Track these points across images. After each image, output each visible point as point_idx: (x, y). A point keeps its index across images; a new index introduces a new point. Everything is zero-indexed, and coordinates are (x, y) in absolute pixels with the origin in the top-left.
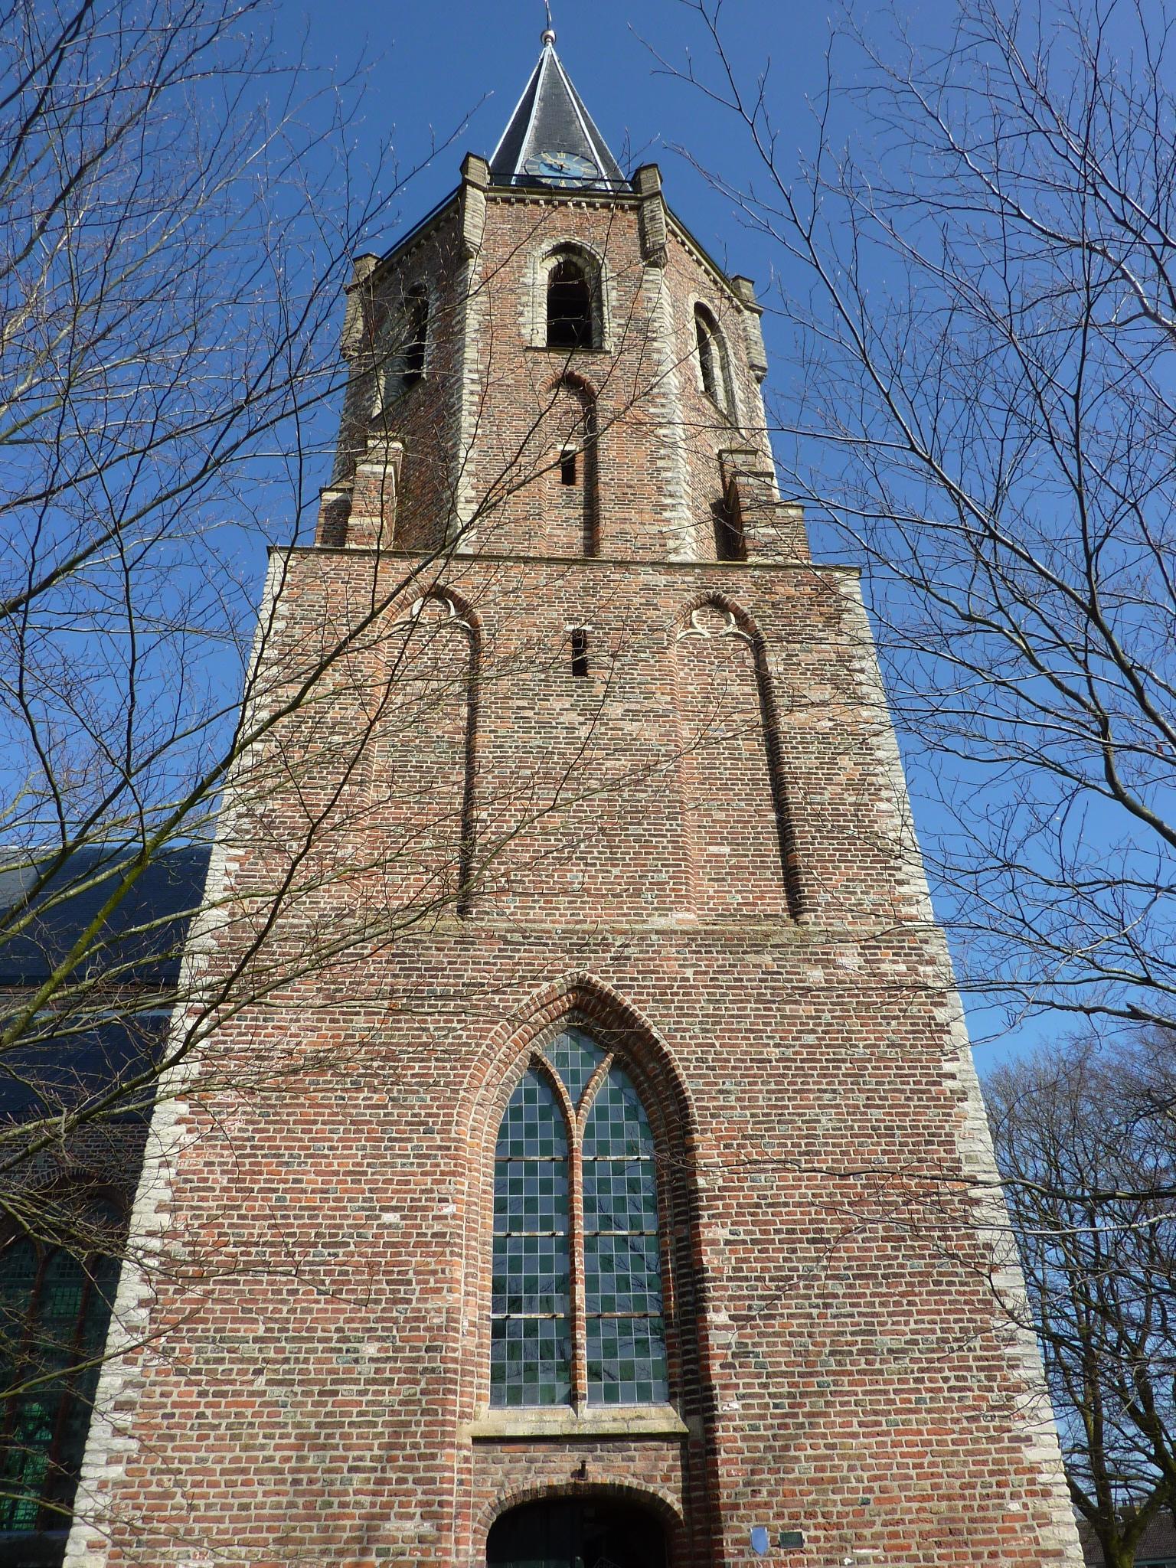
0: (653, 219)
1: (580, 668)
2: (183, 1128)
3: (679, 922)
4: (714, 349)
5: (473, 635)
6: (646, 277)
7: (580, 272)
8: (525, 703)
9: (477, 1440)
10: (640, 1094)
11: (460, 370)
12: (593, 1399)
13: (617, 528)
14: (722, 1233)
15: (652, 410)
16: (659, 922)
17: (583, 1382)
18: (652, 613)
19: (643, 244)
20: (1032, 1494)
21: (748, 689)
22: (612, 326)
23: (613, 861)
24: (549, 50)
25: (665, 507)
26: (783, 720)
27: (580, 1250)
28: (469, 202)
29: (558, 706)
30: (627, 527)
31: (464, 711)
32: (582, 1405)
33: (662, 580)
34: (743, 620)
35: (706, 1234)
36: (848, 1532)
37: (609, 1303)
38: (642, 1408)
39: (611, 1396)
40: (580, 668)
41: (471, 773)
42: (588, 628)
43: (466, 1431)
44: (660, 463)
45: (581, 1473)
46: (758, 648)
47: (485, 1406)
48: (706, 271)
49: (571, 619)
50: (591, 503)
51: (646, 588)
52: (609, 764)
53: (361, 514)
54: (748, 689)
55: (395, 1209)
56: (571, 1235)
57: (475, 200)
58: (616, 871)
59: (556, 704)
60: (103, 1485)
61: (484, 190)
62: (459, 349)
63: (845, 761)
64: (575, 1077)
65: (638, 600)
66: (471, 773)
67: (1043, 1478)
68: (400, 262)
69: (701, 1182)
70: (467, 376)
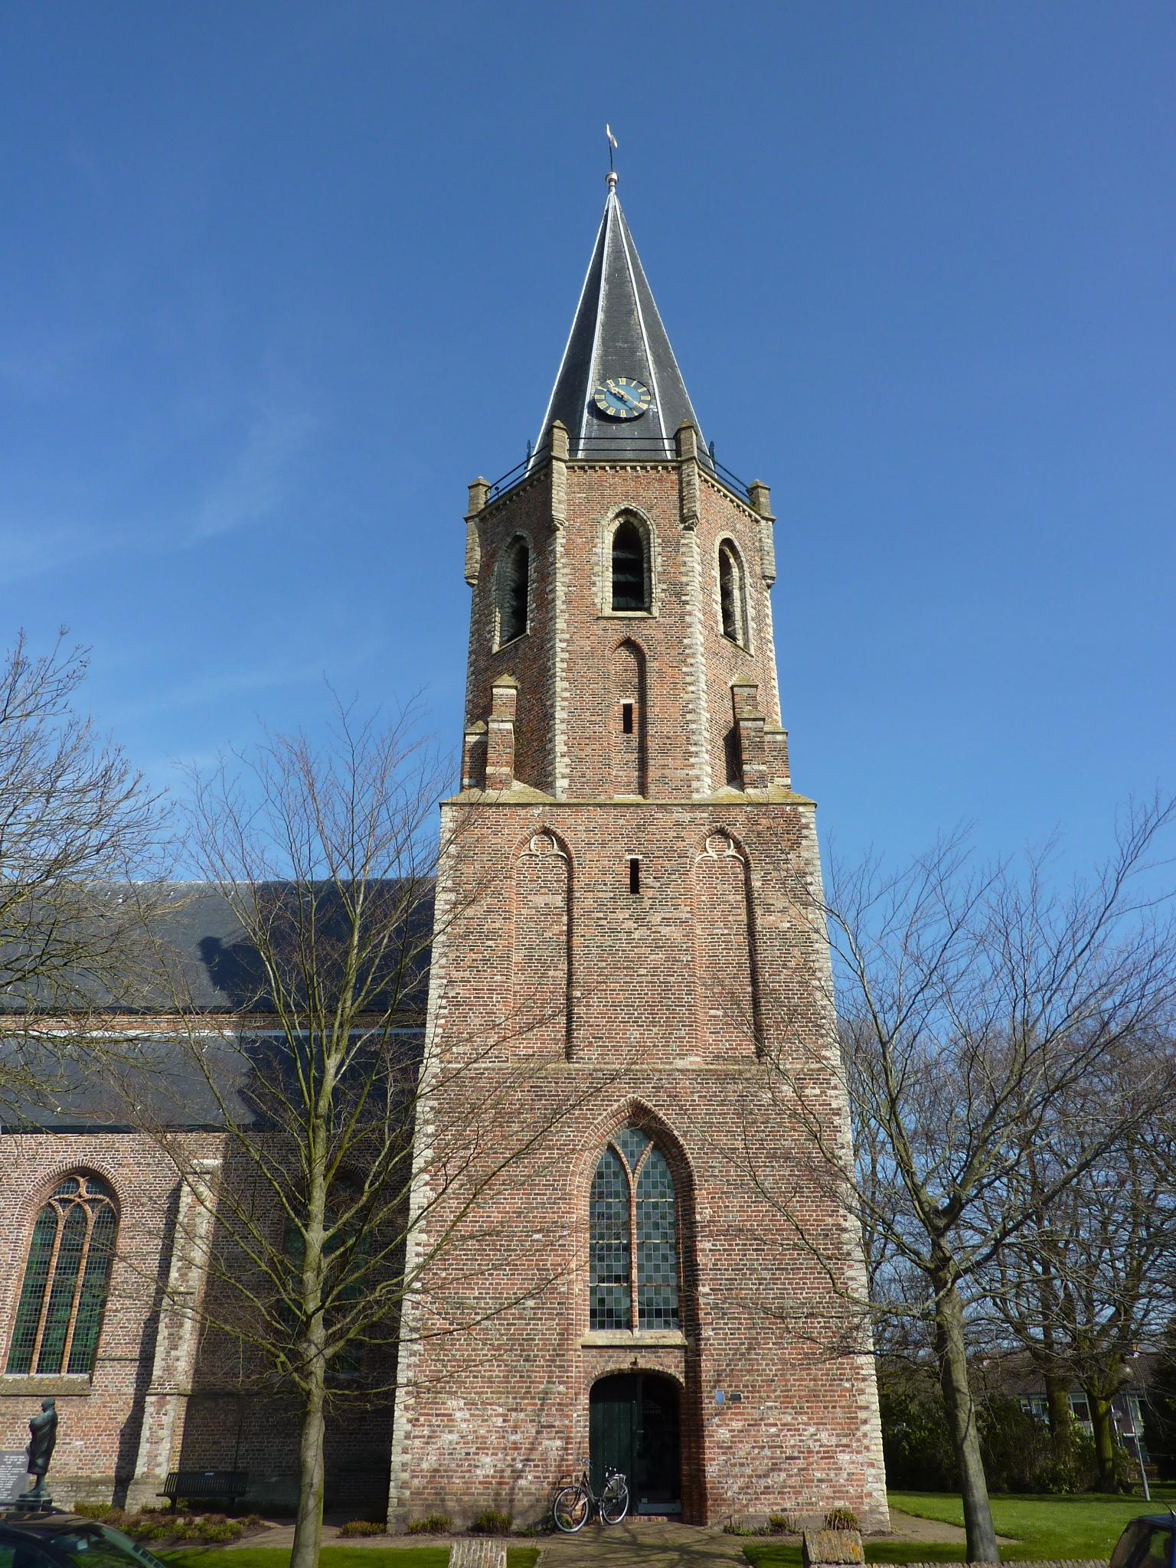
0: (689, 483)
1: (635, 886)
2: (428, 1188)
3: (691, 1063)
4: (735, 571)
5: (569, 861)
6: (683, 541)
7: (635, 530)
8: (601, 915)
9: (583, 1347)
10: (668, 1164)
11: (553, 639)
12: (642, 1326)
13: (659, 773)
14: (708, 1245)
15: (684, 669)
16: (680, 1064)
17: (636, 1319)
18: (680, 844)
19: (681, 509)
20: (857, 1379)
21: (739, 898)
22: (658, 590)
23: (653, 1023)
24: (613, 201)
25: (691, 754)
26: (759, 921)
27: (634, 1251)
28: (555, 437)
29: (621, 916)
30: (667, 772)
31: (565, 918)
32: (636, 1330)
33: (687, 817)
34: (738, 846)
35: (700, 1246)
36: (764, 1395)
37: (649, 1278)
38: (666, 1332)
39: (650, 1326)
40: (635, 886)
41: (570, 963)
42: (640, 857)
43: (580, 1341)
44: (689, 717)
45: (635, 1363)
46: (747, 866)
47: (587, 1329)
48: (732, 501)
49: (630, 851)
50: (643, 749)
51: (678, 824)
52: (652, 957)
53: (493, 764)
54: (739, 898)
55: (539, 1231)
56: (630, 1243)
57: (559, 468)
58: (655, 1030)
59: (621, 915)
60: (409, 1366)
61: (565, 462)
62: (551, 619)
63: (796, 952)
64: (632, 1155)
65: (672, 834)
66: (570, 963)
67: (863, 1372)
68: (505, 504)
69: (698, 1217)
70: (560, 645)
